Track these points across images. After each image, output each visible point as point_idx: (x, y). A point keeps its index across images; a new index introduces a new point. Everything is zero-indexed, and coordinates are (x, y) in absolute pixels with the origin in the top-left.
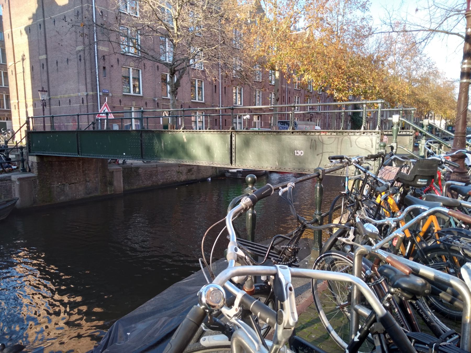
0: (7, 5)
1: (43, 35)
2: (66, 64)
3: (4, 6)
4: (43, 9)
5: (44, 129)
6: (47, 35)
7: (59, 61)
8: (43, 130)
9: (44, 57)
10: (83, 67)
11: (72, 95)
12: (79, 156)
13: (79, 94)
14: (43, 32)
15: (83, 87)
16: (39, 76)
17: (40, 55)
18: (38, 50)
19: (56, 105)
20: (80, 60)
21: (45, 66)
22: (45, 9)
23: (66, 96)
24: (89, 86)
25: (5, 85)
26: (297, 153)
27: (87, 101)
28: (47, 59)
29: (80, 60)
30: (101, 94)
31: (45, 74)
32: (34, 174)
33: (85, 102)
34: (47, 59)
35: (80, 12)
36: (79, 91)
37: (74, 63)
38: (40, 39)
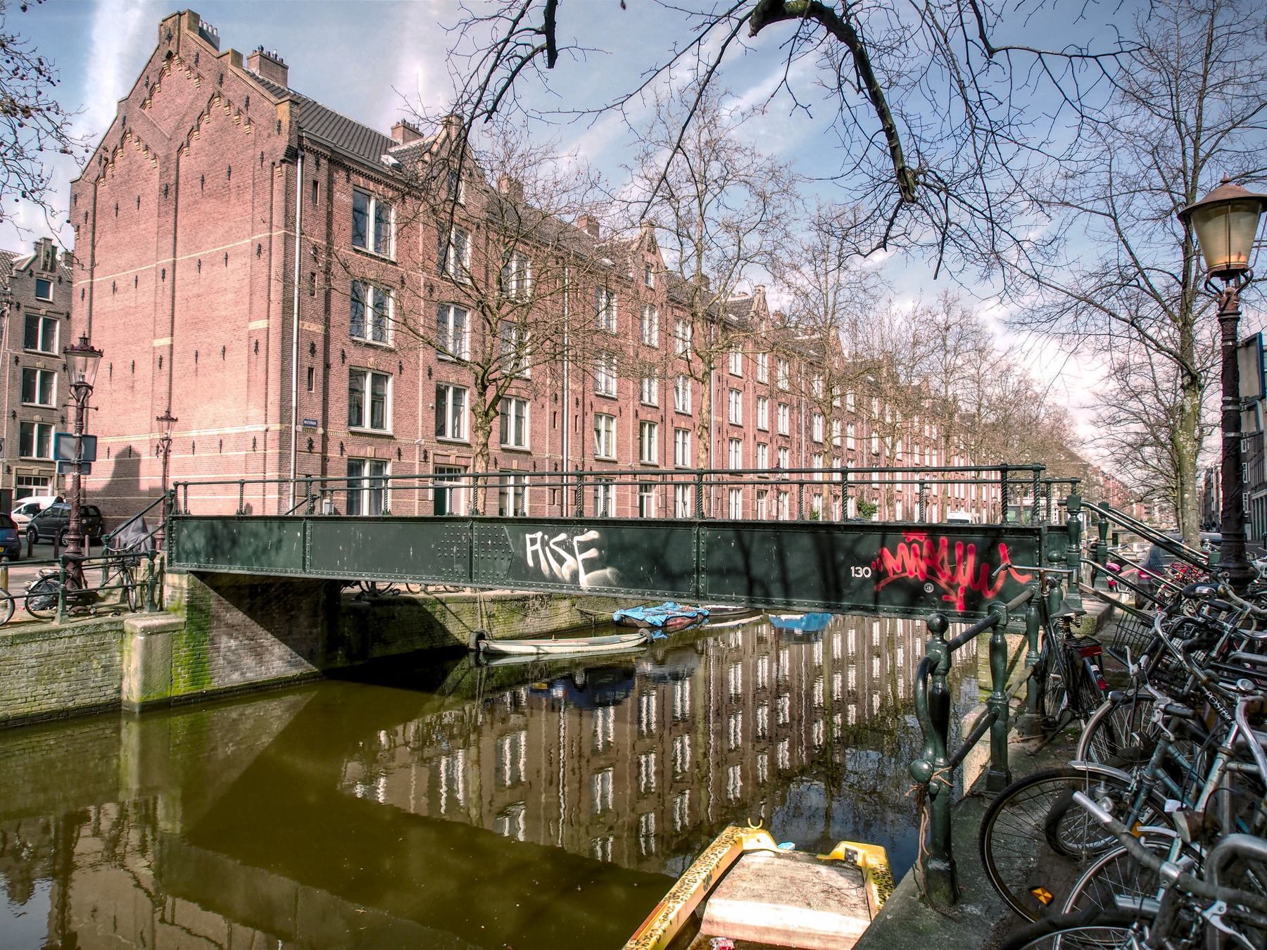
0: (90, 227)
1: (169, 292)
2: (219, 358)
3: (82, 230)
4: (175, 238)
5: (641, 515)
6: (178, 294)
7: (201, 352)
8: (497, 515)
9: (166, 341)
10: (261, 367)
11: (228, 430)
12: (303, 575)
13: (247, 429)
14: (170, 286)
15: (256, 412)
16: (149, 383)
17: (155, 336)
18: (151, 327)
19: (184, 451)
20: (256, 350)
21: (166, 363)
22: (179, 235)
23: (214, 432)
24: (274, 410)
25: (373, 426)
26: (857, 572)
27: (801, 472)
28: (172, 346)
29: (256, 350)
30: (300, 428)
31: (165, 380)
32: (180, 618)
33: (260, 446)
34: (172, 346)
35: (266, 246)
36: (246, 421)
37: (239, 354)
38: (159, 301)
